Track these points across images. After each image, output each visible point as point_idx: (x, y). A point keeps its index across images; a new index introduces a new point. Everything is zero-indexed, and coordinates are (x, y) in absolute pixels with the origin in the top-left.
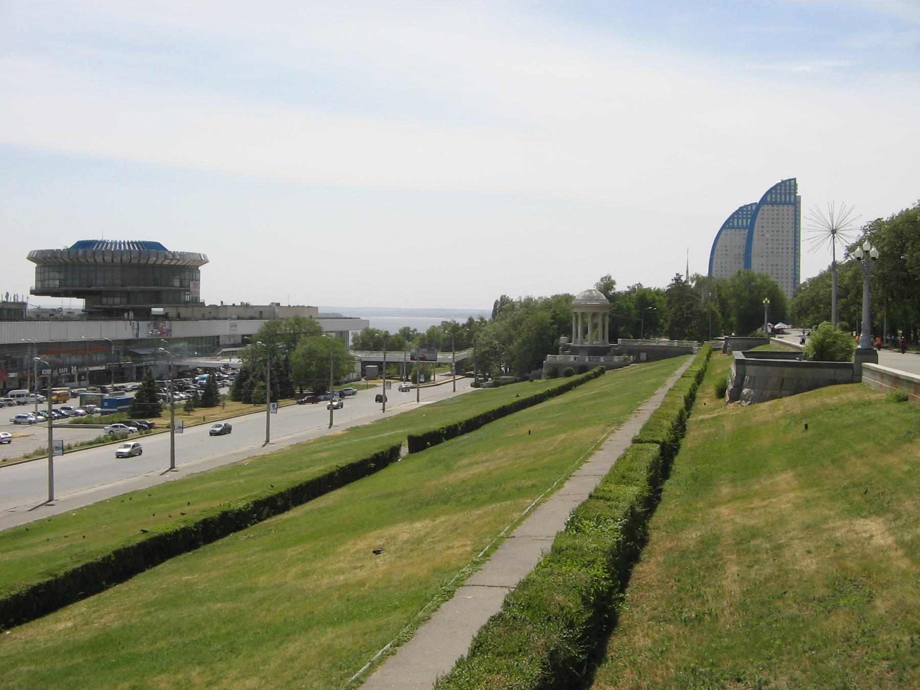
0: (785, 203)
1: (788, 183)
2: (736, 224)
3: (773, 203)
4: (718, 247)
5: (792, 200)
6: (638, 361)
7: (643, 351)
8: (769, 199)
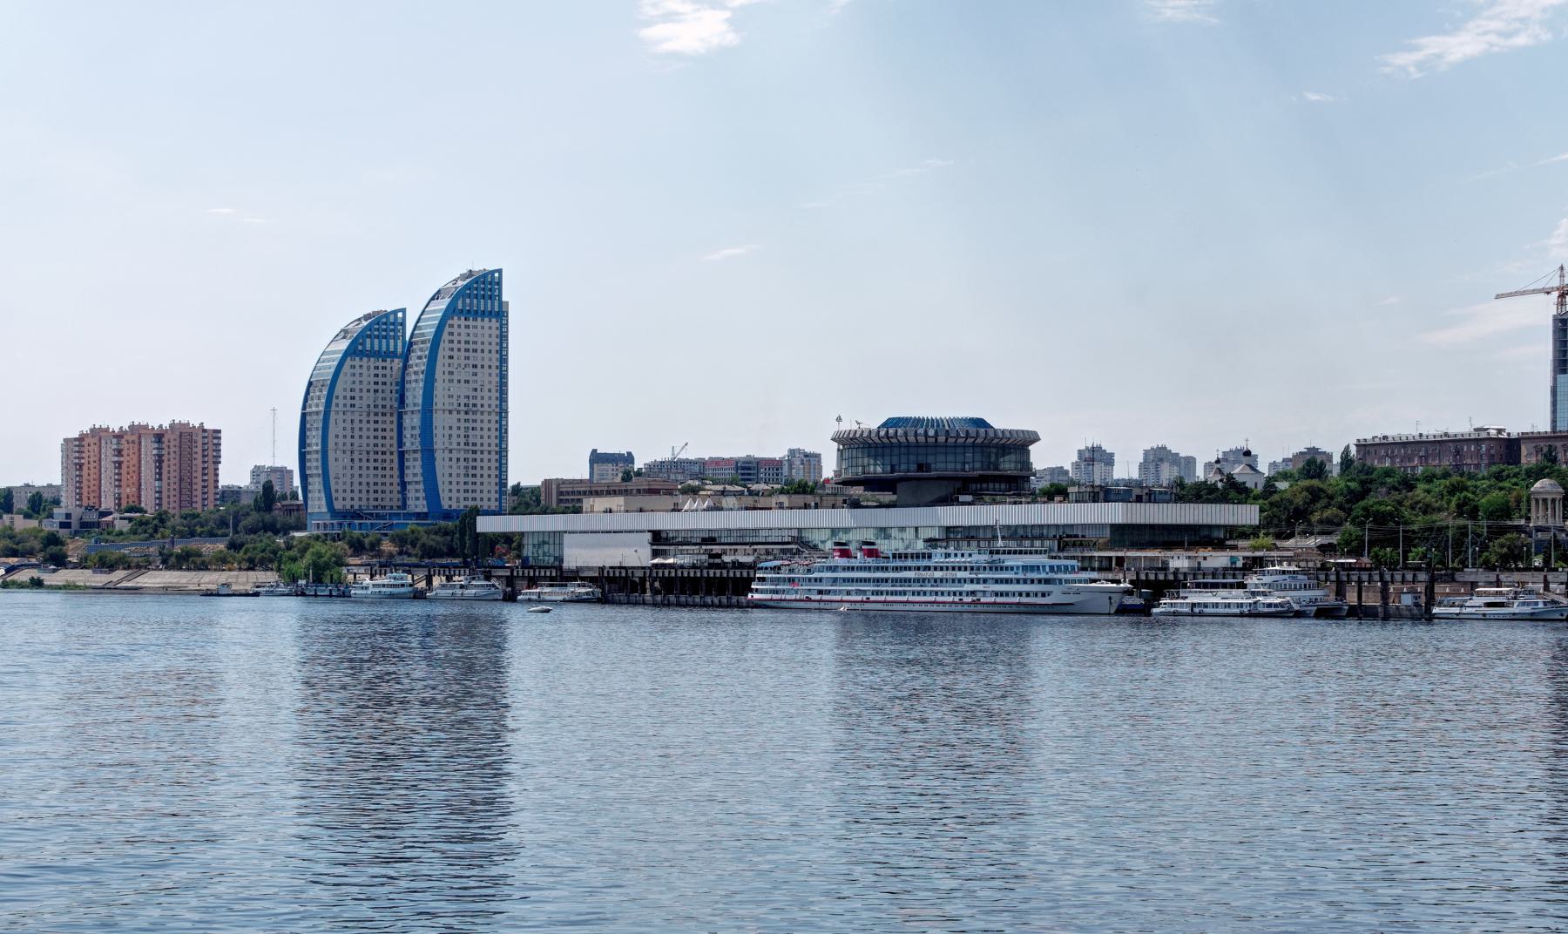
2: (368, 347)
4: (338, 390)
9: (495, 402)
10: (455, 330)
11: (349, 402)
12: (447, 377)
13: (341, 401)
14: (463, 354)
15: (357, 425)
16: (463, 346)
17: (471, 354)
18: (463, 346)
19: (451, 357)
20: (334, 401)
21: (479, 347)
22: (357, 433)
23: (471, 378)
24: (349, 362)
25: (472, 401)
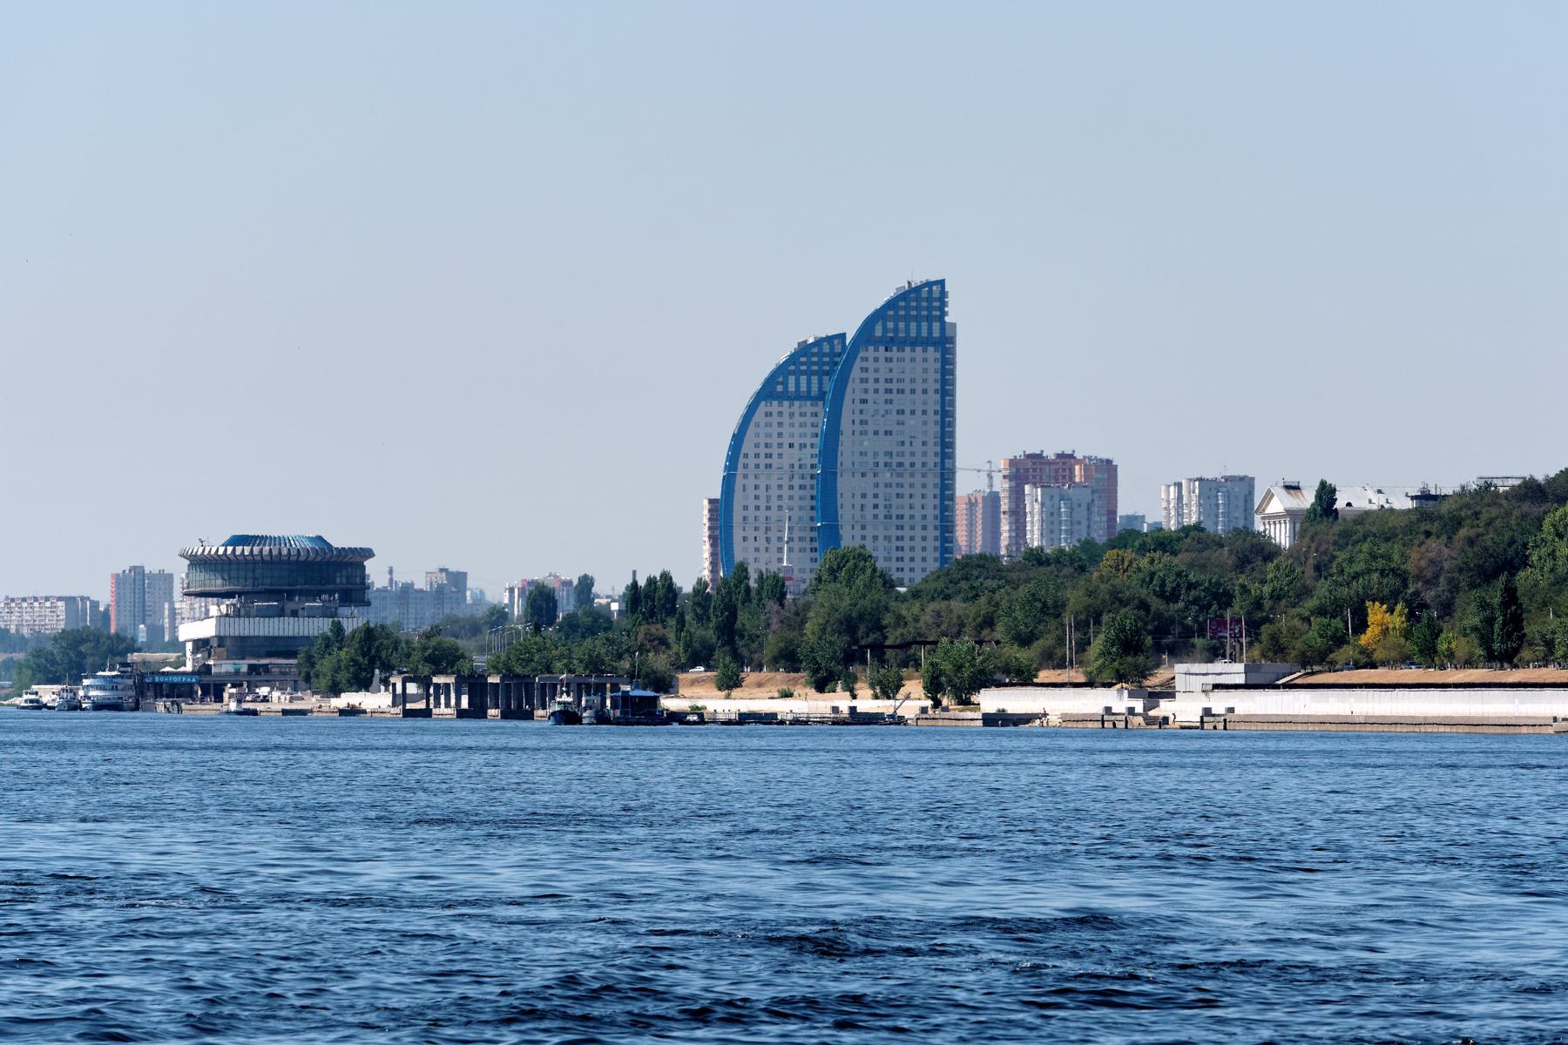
3: (889, 343)
4: (748, 447)
5: (936, 334)
8: (878, 332)
9: (932, 460)
10: (871, 365)
11: (762, 461)
12: (858, 427)
13: (752, 461)
14: (882, 396)
15: (774, 492)
16: (882, 386)
17: (894, 396)
18: (882, 386)
19: (864, 401)
20: (742, 461)
21: (907, 386)
22: (774, 503)
23: (895, 428)
25: (896, 460)
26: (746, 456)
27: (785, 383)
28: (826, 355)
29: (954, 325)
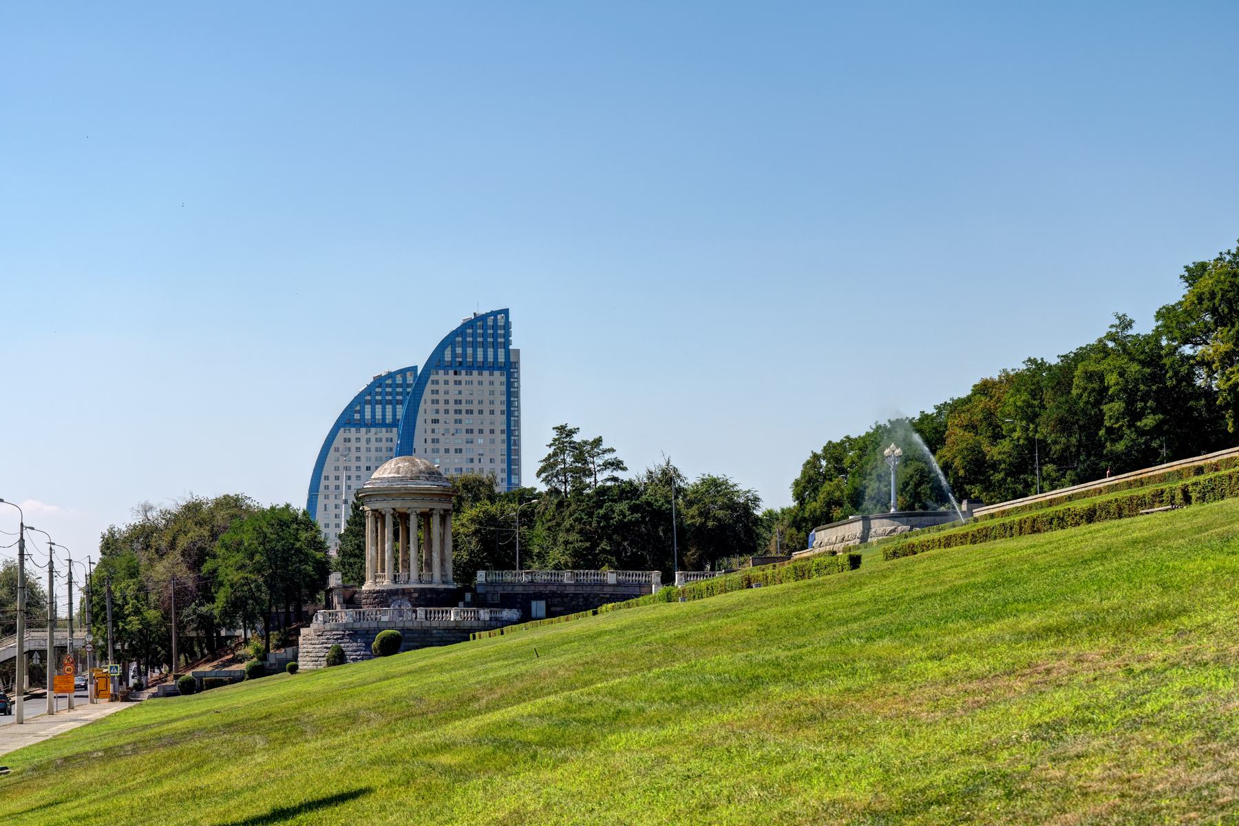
0: (481, 367)
1: (490, 321)
2: (368, 415)
3: (458, 366)
4: (328, 470)
5: (501, 359)
6: (526, 617)
7: (539, 596)
8: (448, 356)
10: (441, 387)
12: (430, 446)
17: (463, 416)
19: (436, 421)
20: (323, 483)
24: (341, 434)
26: (327, 478)
27: (362, 412)
28: (398, 386)
29: (518, 351)
